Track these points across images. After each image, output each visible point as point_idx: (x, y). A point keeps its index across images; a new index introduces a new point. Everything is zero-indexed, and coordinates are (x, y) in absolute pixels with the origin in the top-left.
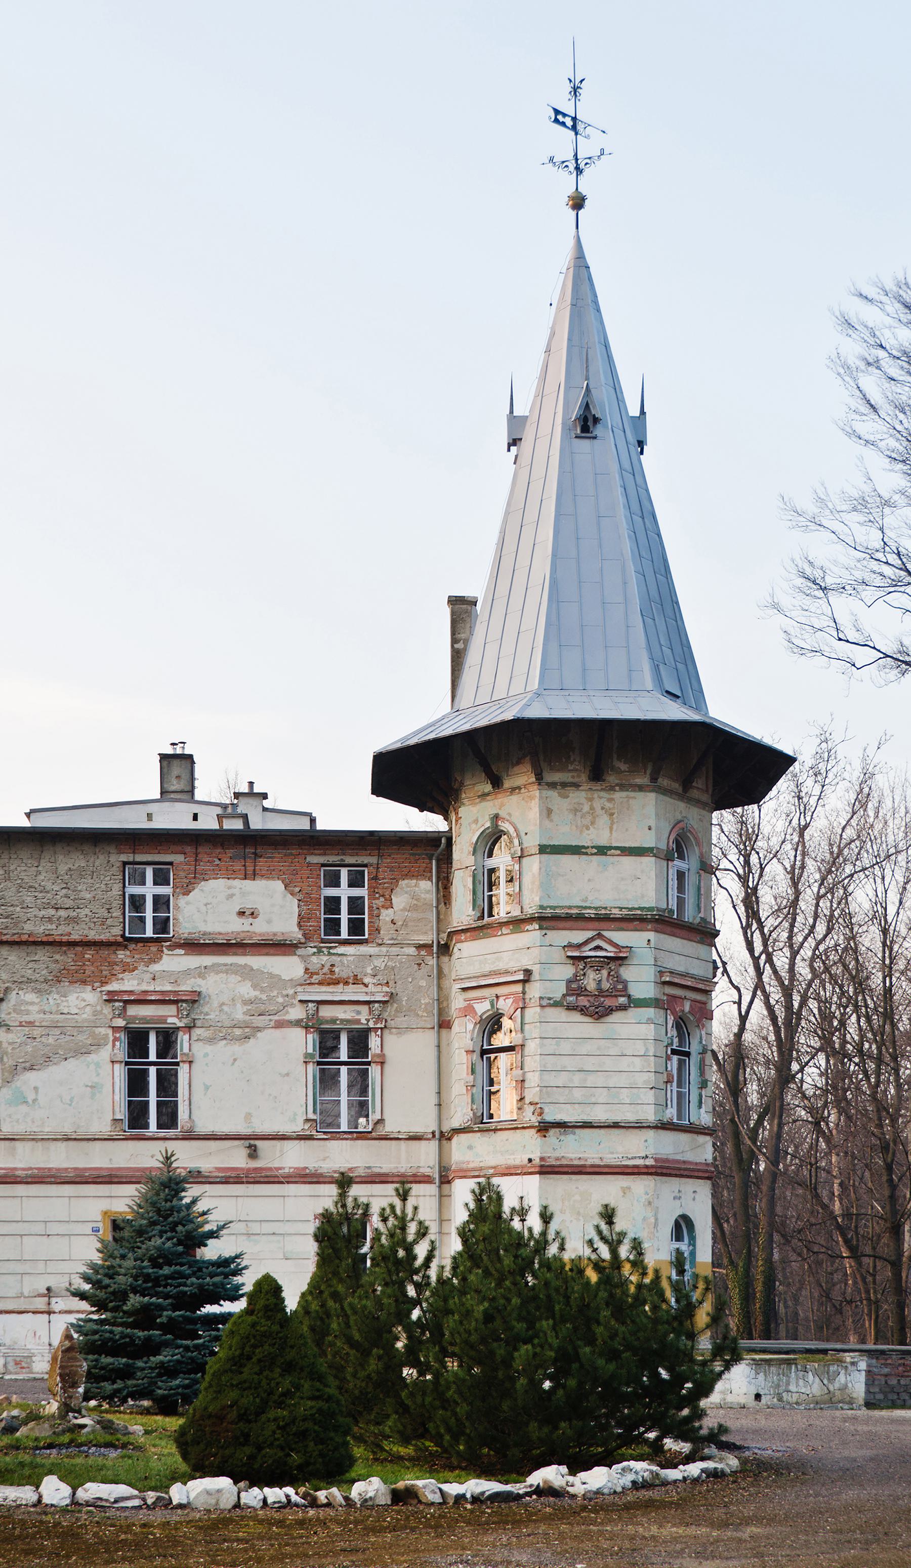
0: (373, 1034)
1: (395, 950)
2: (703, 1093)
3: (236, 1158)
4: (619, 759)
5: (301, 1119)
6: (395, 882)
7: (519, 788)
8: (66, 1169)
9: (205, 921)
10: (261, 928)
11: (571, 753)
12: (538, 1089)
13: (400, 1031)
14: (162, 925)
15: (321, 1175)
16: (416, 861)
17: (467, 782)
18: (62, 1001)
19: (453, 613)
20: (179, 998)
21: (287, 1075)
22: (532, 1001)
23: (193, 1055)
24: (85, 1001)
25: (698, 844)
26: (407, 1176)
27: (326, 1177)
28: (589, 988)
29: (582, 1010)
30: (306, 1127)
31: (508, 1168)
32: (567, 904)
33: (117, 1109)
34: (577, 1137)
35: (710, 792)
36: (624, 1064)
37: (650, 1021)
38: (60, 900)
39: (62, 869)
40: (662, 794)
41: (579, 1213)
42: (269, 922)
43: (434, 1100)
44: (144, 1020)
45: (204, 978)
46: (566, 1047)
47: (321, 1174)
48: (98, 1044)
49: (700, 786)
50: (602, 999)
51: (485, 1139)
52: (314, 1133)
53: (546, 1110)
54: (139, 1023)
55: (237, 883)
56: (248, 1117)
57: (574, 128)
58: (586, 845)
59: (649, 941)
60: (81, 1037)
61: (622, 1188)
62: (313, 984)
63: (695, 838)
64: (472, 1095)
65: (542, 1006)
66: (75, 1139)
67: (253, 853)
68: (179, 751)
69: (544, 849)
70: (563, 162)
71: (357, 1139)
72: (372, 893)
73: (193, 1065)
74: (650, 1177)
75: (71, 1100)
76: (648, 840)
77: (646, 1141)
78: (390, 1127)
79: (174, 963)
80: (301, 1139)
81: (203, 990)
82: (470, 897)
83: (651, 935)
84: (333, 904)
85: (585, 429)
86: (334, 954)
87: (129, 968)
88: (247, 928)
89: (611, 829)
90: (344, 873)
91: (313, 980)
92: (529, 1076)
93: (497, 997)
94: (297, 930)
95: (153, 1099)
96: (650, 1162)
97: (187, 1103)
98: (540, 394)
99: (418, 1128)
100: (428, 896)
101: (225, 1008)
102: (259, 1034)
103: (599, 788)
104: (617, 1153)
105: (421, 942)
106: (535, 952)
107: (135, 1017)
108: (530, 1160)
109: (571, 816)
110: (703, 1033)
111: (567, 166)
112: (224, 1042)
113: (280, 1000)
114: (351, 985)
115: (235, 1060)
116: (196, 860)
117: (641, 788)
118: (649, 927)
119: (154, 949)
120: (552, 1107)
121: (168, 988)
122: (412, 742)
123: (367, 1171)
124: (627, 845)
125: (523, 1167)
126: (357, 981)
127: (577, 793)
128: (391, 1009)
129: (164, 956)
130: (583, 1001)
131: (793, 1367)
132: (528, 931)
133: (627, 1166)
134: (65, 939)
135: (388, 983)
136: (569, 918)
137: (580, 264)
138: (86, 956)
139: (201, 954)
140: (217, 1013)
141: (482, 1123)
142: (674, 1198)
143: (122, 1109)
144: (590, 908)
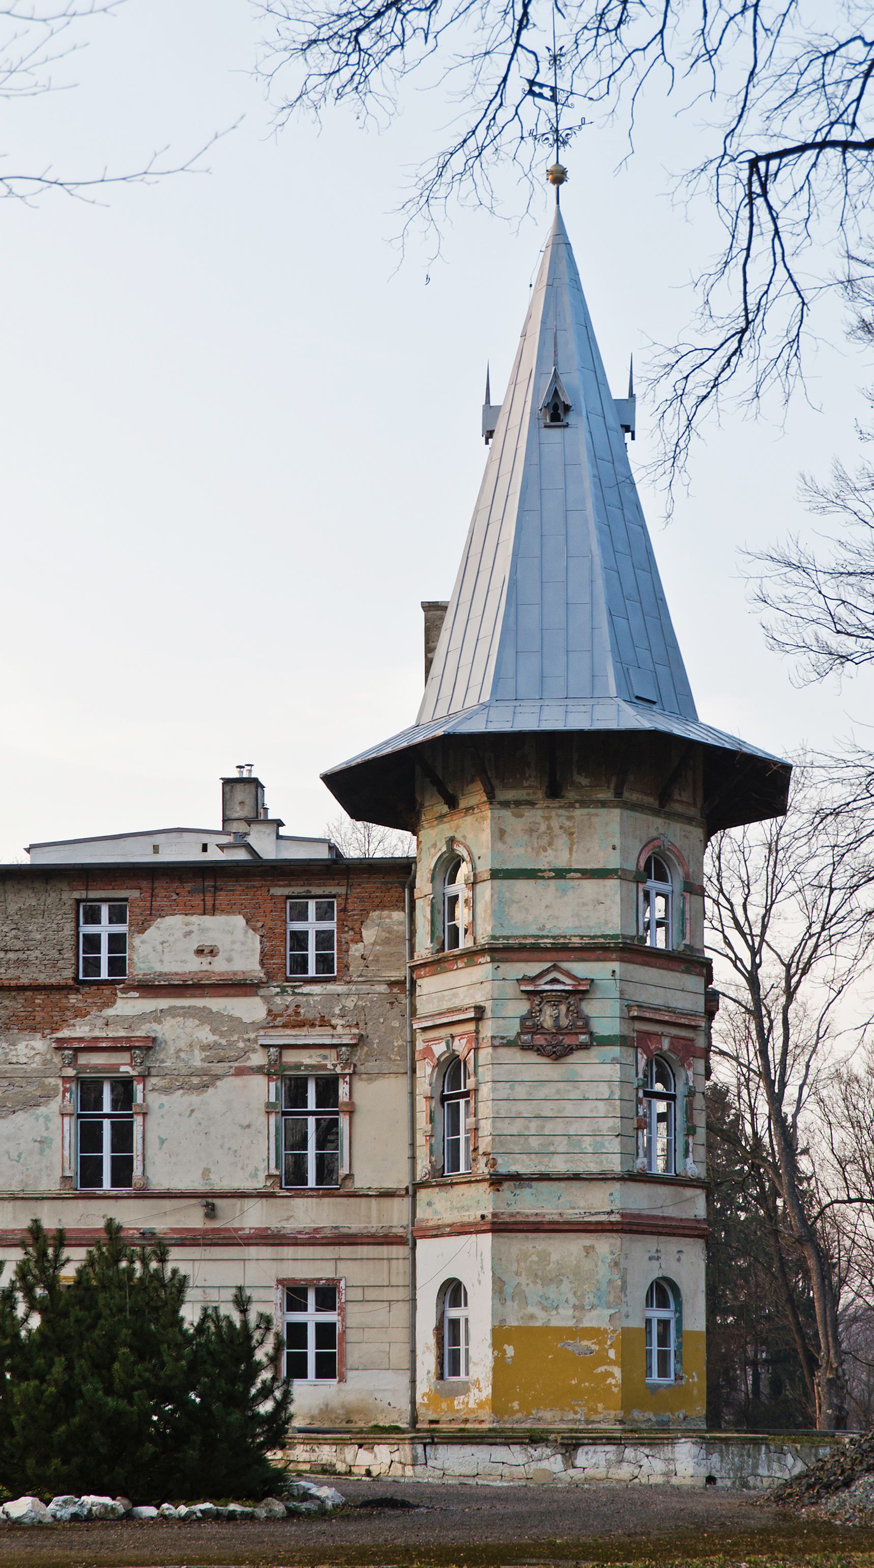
0: (341, 1081)
1: (365, 988)
2: (691, 1140)
3: (193, 1218)
4: (579, 773)
5: (262, 1175)
6: (364, 914)
7: (472, 808)
8: (13, 1231)
9: (161, 961)
10: (220, 966)
11: (527, 769)
12: (490, 1138)
13: (372, 1077)
14: (117, 966)
15: (284, 1236)
16: (388, 890)
17: (426, 804)
18: (11, 1050)
19: (426, 620)
20: (132, 1044)
21: (249, 1126)
22: (485, 1041)
23: (147, 1105)
24: (34, 1049)
25: (682, 864)
26: (377, 1237)
27: (289, 1238)
28: (545, 1025)
29: (538, 1050)
30: (268, 1184)
31: (463, 1225)
32: (522, 933)
33: (67, 1166)
34: (534, 1191)
35: (699, 806)
36: (586, 1109)
37: (614, 1061)
38: (10, 942)
39: (12, 908)
40: (628, 809)
41: (536, 1275)
42: (229, 960)
43: (407, 1153)
44: (96, 1069)
45: (160, 1022)
46: (521, 1091)
47: (284, 1235)
48: (48, 1096)
49: (685, 800)
50: (561, 1038)
51: (443, 1194)
52: (277, 1190)
53: (500, 1161)
54: (90, 1072)
55: (195, 919)
56: (206, 1173)
57: (553, 98)
58: (543, 868)
59: (614, 972)
60: (29, 1089)
61: (584, 1247)
62: (277, 1027)
63: (677, 857)
64: (431, 1145)
65: (494, 1047)
66: (22, 1198)
67: (212, 886)
68: (245, 775)
69: (495, 874)
70: (544, 134)
71: (323, 1196)
72: (341, 926)
73: (148, 1118)
74: (614, 1235)
75: (19, 1156)
76: (613, 861)
77: (611, 1194)
78: (360, 1182)
79: (128, 1006)
80: (262, 1197)
81: (159, 1035)
82: (428, 928)
83: (616, 966)
84: (299, 939)
85: (555, 417)
86: (299, 994)
87: (81, 1013)
88: (205, 967)
89: (571, 850)
90: (312, 905)
91: (276, 1023)
92: (482, 1123)
93: (453, 1037)
94: (260, 968)
95: (107, 1154)
96: (615, 1218)
97: (140, 1158)
98: (514, 383)
99: (390, 1184)
100: (401, 928)
101: (182, 1055)
102: (218, 1083)
103: (557, 805)
104: (578, 1208)
105: (393, 979)
106: (488, 986)
107: (86, 1066)
108: (483, 1217)
109: (526, 837)
110: (690, 1073)
111: (547, 139)
112: (181, 1091)
113: (241, 1045)
114: (317, 1028)
115: (192, 1111)
116: (152, 896)
117: (604, 804)
118: (614, 956)
119: (107, 992)
120: (506, 1157)
121: (122, 1033)
122: (353, 763)
123: (334, 1231)
124: (589, 867)
125: (476, 1224)
126: (324, 1022)
127: (533, 812)
128: (361, 1053)
129: (118, 1000)
130: (540, 1040)
131: (763, 1448)
132: (480, 964)
133: (589, 1223)
134: (13, 983)
135: (357, 1024)
136: (522, 948)
137: (560, 241)
138: (37, 1001)
139: (157, 996)
140: (174, 1060)
141: (443, 1177)
142: (650, 1259)
143: (73, 1166)
144: (547, 937)
